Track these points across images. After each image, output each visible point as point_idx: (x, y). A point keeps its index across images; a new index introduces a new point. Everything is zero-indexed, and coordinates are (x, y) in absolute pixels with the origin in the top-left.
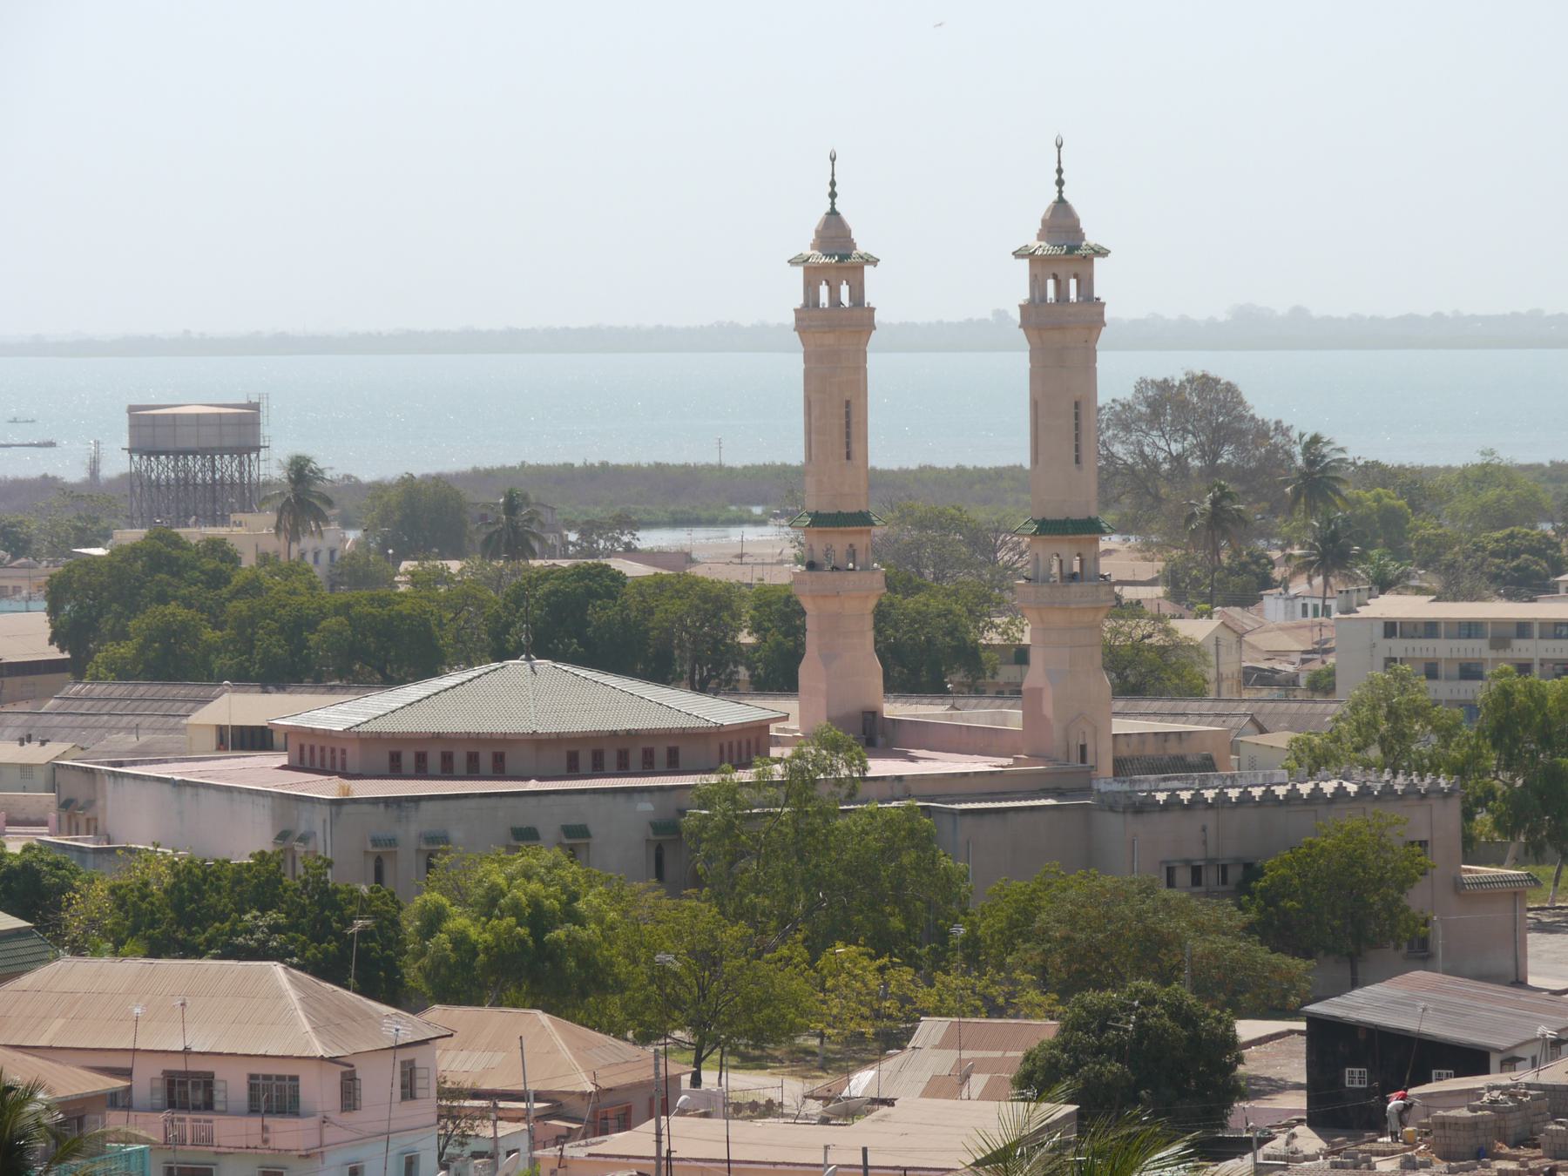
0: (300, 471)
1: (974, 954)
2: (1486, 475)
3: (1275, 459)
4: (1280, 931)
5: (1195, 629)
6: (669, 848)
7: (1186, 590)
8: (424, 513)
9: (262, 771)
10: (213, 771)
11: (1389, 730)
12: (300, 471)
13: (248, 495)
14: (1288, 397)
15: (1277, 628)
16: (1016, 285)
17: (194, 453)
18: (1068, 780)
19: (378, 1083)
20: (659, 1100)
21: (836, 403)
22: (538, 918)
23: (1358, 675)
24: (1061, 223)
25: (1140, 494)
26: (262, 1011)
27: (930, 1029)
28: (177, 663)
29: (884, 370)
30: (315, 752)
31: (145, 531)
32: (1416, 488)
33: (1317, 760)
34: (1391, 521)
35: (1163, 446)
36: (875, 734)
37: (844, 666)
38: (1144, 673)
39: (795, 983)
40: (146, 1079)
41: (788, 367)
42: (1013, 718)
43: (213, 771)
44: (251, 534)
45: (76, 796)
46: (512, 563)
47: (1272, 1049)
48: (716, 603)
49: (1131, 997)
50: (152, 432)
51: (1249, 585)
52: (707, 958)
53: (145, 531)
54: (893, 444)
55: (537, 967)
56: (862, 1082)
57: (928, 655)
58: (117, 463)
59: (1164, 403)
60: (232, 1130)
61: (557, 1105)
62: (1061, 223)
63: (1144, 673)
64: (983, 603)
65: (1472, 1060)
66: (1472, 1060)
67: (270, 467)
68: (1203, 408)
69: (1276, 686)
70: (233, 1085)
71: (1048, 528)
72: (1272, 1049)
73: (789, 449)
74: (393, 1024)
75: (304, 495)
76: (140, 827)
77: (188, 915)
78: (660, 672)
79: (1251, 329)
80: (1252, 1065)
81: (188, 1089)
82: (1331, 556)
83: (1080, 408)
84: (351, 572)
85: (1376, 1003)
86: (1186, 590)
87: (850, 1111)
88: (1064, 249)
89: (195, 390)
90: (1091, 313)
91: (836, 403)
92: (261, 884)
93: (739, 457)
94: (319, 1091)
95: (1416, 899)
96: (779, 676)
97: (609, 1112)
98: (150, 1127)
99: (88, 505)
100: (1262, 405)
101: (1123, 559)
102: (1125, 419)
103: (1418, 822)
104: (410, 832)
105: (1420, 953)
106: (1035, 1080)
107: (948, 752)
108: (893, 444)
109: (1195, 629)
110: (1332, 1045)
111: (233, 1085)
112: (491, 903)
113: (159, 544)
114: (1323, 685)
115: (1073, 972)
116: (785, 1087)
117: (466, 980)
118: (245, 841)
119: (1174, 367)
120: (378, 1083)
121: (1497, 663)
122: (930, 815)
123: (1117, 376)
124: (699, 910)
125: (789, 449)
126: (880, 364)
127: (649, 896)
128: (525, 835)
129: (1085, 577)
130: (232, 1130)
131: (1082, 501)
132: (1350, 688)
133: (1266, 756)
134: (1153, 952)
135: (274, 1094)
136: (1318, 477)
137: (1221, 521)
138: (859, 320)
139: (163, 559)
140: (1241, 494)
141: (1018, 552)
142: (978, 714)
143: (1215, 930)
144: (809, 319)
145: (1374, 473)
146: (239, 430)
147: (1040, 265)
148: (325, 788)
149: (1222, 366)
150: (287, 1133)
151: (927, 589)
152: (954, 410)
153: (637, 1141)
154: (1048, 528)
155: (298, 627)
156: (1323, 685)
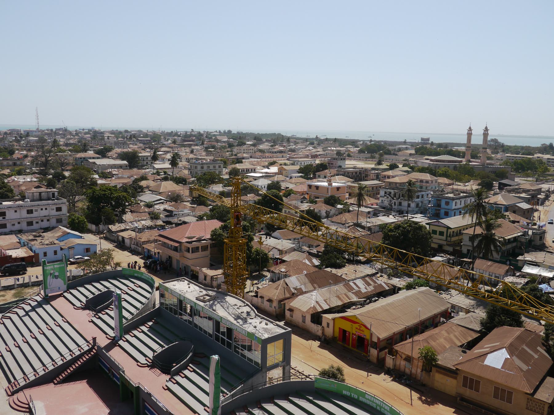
0: (432, 142)
1: (475, 176)
2: (515, 146)
3: (500, 144)
4: (497, 176)
5: (493, 156)
6: (455, 168)
7: (492, 153)
8: (440, 145)
9: (428, 161)
10: (425, 161)
11: (506, 163)
12: (432, 142)
13: (428, 144)
14: (501, 140)
15: (499, 156)
16: (483, 132)
17: (425, 141)
18: (483, 165)
19: (434, 182)
20: (453, 184)
21: (469, 139)
22: (446, 172)
23: (504, 159)
24: (486, 128)
25: (490, 146)
26: (427, 177)
27: (472, 181)
28: (423, 154)
29: (473, 137)
30: (431, 160)
31: (518, 258)
32: (510, 147)
33: (501, 165)
34: (508, 149)
35: (492, 143)
36: (470, 161)
37: (468, 156)
38: (489, 158)
39: (462, 177)
40: (419, 180)
41: (466, 137)
42: (480, 161)
43: (425, 161)
44: (428, 146)
45: (416, 162)
46: (446, 149)
47: (496, 184)
48: (460, 152)
49: (487, 180)
50: (422, 139)
51: (497, 153)
52: (457, 175)
53: (518, 258)
54: (473, 142)
55: (445, 175)
56: (467, 184)
57: (474, 156)
58: (420, 141)
59: (492, 140)
60: (424, 184)
61: (446, 184)
62: (486, 128)
63: (489, 158)
64: (478, 153)
65: (510, 186)
66: (510, 186)
67: (430, 142)
68: (495, 141)
69: (498, 160)
70: (424, 181)
71: (483, 148)
72: (496, 184)
73: (466, 142)
74: (436, 178)
75: (432, 144)
76: (420, 165)
77: (422, 170)
78: (455, 156)
79: (499, 136)
80: (494, 185)
81: (421, 181)
82: (503, 151)
83: (486, 140)
84: (435, 149)
85: (503, 181)
86: (492, 153)
87: (466, 186)
88: (486, 129)
89: (425, 137)
90: (488, 134)
91: (469, 139)
92: (427, 168)
93: (462, 142)
94: (430, 182)
95: (507, 175)
96: (463, 157)
97: (449, 185)
98: (419, 183)
99: (418, 144)
100: (499, 141)
101: (488, 151)
102: (489, 141)
103: (508, 170)
104: (437, 166)
105: (507, 178)
106: (479, 185)
107: (475, 163)
108: (473, 142)
109: (493, 156)
110: (500, 184)
111: (424, 181)
112: (443, 171)
113: (176, 262)
114: (502, 160)
115: (481, 178)
116: (462, 184)
117: (440, 176)
118: (426, 166)
119: (493, 138)
120: (434, 182)
121: (515, 159)
122: (473, 167)
123: (489, 138)
124: (457, 172)
125: (466, 142)
126: (472, 137)
127: (453, 171)
128: (445, 167)
129: (486, 152)
130: (424, 184)
131: (486, 146)
132: (504, 160)
133: (497, 165)
134: (488, 177)
135: (427, 182)
136: (503, 146)
137: (496, 148)
138: (471, 134)
139: (422, 147)
140: (497, 147)
141: (481, 150)
142: (477, 160)
143: (493, 176)
144: (468, 134)
145: (507, 146)
146: (428, 139)
147: (485, 131)
148: (432, 163)
149: (497, 138)
150: (428, 184)
151: (474, 151)
152: (477, 140)
153: (451, 187)
154: (483, 148)
155: (431, 152)
156: (502, 160)
